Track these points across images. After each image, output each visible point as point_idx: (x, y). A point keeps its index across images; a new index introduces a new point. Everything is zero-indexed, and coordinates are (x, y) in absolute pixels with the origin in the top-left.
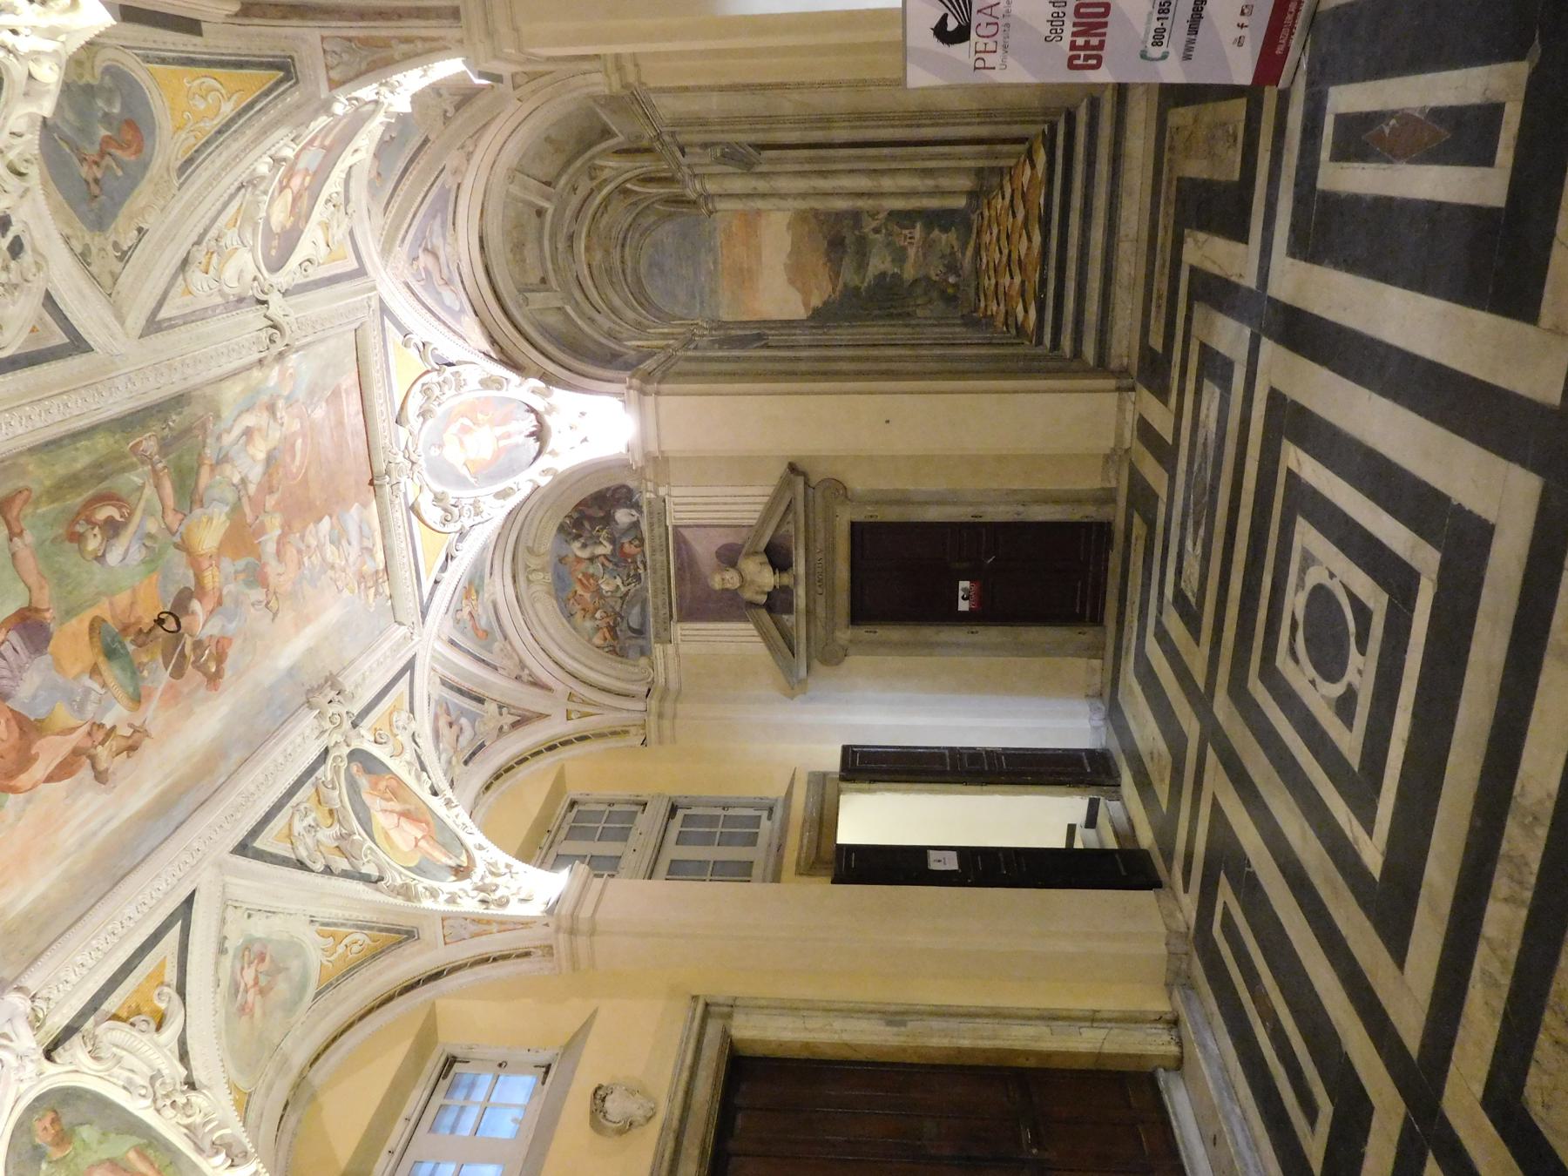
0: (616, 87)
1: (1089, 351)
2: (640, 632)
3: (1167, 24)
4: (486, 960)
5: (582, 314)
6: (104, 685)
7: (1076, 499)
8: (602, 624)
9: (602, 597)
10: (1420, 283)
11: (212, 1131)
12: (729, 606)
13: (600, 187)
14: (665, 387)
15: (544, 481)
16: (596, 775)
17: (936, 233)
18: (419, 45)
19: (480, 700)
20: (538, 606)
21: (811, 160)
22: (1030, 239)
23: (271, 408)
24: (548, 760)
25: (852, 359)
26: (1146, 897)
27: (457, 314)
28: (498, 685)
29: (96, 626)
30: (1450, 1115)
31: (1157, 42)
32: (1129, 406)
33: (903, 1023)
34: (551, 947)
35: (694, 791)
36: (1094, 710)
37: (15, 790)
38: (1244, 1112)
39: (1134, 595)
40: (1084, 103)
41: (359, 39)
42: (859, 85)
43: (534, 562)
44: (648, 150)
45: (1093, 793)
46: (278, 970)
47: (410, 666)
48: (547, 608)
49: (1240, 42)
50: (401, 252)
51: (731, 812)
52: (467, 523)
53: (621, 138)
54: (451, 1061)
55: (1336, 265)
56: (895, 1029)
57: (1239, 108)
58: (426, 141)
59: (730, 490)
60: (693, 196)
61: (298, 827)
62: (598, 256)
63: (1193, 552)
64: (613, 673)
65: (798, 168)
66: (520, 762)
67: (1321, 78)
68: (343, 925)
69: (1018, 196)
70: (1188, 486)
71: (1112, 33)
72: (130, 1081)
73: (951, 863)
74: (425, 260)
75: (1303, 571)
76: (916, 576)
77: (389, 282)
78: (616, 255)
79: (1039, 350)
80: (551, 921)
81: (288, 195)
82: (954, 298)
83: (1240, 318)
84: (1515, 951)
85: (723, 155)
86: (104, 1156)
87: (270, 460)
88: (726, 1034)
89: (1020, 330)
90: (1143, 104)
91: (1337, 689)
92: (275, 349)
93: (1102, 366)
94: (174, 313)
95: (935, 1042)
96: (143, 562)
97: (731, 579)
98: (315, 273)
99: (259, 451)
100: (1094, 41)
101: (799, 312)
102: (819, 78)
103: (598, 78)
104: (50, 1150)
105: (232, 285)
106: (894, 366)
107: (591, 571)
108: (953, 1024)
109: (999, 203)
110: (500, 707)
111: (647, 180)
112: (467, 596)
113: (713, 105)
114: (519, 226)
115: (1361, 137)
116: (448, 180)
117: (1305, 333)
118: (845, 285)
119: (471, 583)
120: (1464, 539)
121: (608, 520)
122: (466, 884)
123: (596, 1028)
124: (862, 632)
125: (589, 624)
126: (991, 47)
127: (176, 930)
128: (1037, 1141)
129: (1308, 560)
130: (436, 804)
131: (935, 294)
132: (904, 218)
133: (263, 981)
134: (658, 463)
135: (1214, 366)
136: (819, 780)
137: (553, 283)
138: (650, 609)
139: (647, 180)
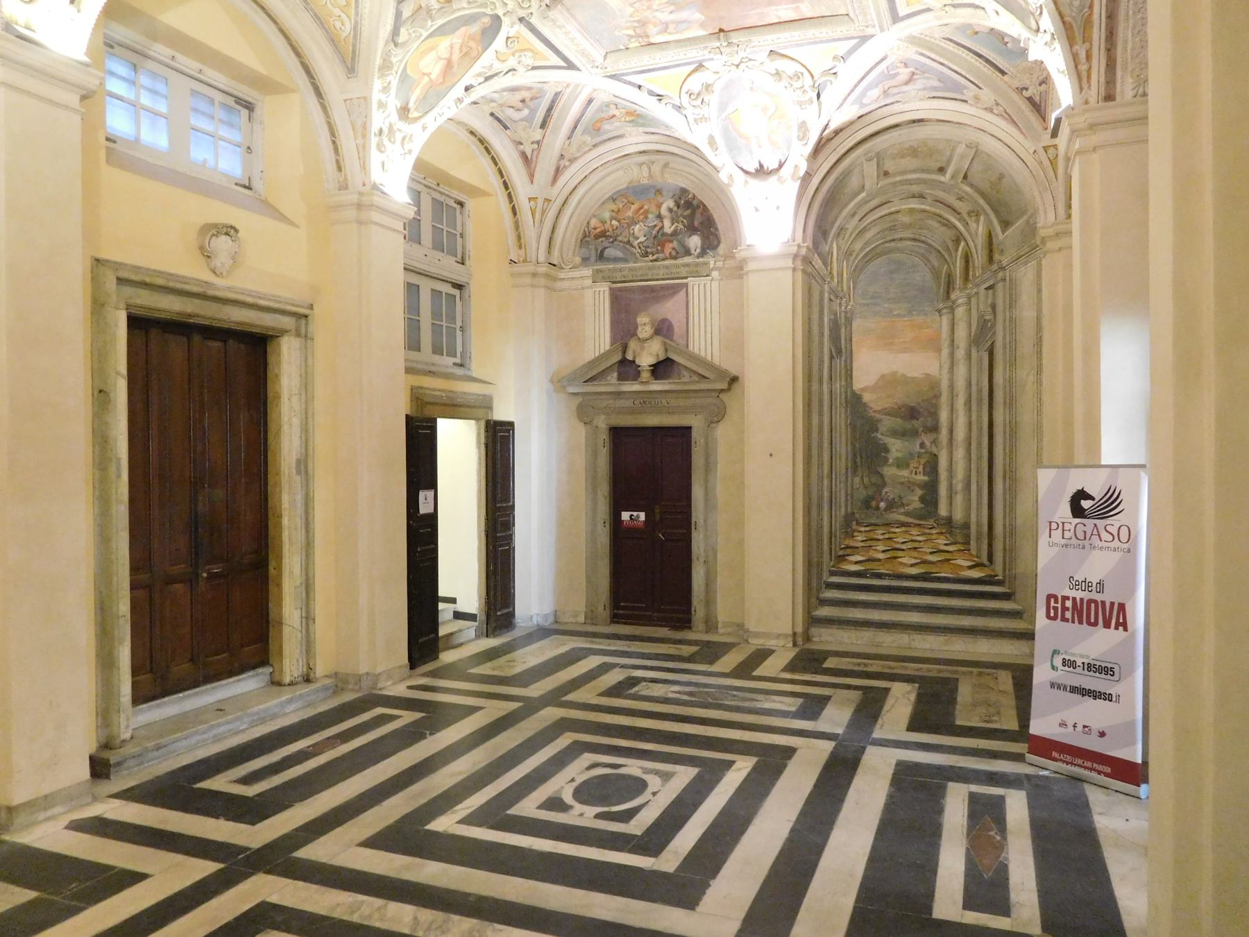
0: (1042, 233)
1: (825, 612)
2: (601, 257)
3: (1079, 670)
4: (333, 134)
5: (859, 206)
7: (709, 602)
8: (607, 226)
9: (629, 225)
10: (875, 859)
12: (623, 330)
13: (961, 220)
14: (799, 275)
15: (723, 177)
16: (485, 222)
17: (919, 492)
18: (1083, 68)
19: (543, 125)
20: (620, 173)
21: (980, 391)
22: (912, 565)
25: (821, 427)
26: (405, 660)
27: (859, 101)
28: (556, 141)
30: (254, 878)
32: (781, 643)
33: (299, 472)
35: (474, 302)
36: (546, 617)
38: (243, 731)
41: (1090, 15)
42: (1038, 430)
43: (656, 169)
44: (991, 259)
45: (482, 617)
47: (570, 66)
50: (911, 53)
51: (459, 333)
52: (689, 111)
53: (1001, 237)
54: (249, 107)
55: (890, 797)
57: (1010, 723)
58: (1003, 73)
59: (716, 331)
60: (953, 297)
62: (906, 219)
63: (670, 691)
64: (568, 234)
65: (974, 382)
66: (493, 159)
67: (1036, 788)
68: (357, 13)
69: (948, 556)
70: (719, 687)
74: (905, 73)
76: (650, 484)
77: (891, 44)
78: (907, 234)
80: (368, 187)
84: (377, 925)
88: (283, 332)
89: (842, 558)
90: (1016, 652)
91: (568, 798)
93: (813, 621)
97: (645, 331)
100: (1068, 615)
101: (858, 385)
103: (1051, 217)
107: (650, 216)
108: (300, 510)
109: (941, 542)
110: (538, 142)
111: (967, 259)
112: (629, 113)
113: (1026, 314)
114: (931, 153)
115: (986, 814)
117: (839, 772)
118: (879, 421)
121: (692, 230)
122: (394, 117)
124: (604, 436)
125: (607, 215)
126: (1067, 535)
128: (212, 576)
130: (458, 90)
131: (871, 492)
132: (932, 467)
134: (739, 270)
135: (813, 706)
136: (486, 404)
137: (885, 182)
139: (967, 259)
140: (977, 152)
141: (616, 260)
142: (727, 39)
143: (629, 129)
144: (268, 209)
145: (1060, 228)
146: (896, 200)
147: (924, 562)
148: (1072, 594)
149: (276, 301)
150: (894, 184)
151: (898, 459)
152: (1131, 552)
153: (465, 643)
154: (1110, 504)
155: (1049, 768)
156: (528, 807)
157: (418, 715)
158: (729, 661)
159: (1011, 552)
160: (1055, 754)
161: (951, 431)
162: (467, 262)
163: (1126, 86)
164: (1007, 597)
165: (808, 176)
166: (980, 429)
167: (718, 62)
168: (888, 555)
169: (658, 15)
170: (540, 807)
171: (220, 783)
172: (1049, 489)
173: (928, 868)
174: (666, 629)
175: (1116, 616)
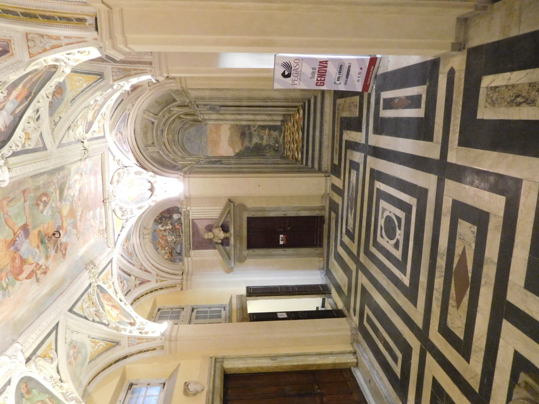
0: (179, 88)
1: (316, 166)
2: (180, 254)
3: (341, 76)
4: (141, 352)
5: (165, 154)
6: (40, 252)
7: (314, 209)
8: (168, 251)
9: (168, 243)
10: (407, 136)
11: (69, 395)
12: (209, 244)
13: (172, 116)
14: (191, 175)
15: (153, 204)
16: (165, 300)
17: (272, 132)
18: (139, 71)
19: (130, 275)
20: (147, 246)
21: (235, 110)
22: (299, 134)
23: (81, 174)
24: (150, 296)
26: (344, 319)
28: (135, 271)
29: (40, 232)
30: (431, 339)
31: (338, 80)
32: (329, 181)
33: (276, 360)
34: (163, 346)
35: (199, 304)
36: (321, 273)
37: (18, 280)
38: (377, 371)
39: (333, 235)
40: (313, 98)
41: (122, 69)
43: (146, 232)
45: (323, 296)
46: (79, 352)
47: (111, 261)
48: (149, 246)
49: (358, 81)
50: (114, 132)
51: (212, 309)
52: (128, 216)
53: (179, 102)
54: (131, 385)
55: (386, 135)
56: (274, 361)
57: (357, 99)
58: (123, 100)
59: (209, 208)
60: (200, 119)
61: (85, 306)
62: (171, 136)
63: (351, 217)
64: (170, 267)
65: (232, 112)
66: (141, 296)
67: (380, 89)
68: (98, 339)
69: (295, 122)
70: (348, 200)
71: (327, 78)
72: (45, 377)
73: (285, 316)
74: (119, 135)
75: (383, 213)
76: (268, 233)
77: (111, 139)
78: (176, 136)
79: (302, 166)
80: (162, 337)
81: (93, 111)
82: (278, 150)
83: (361, 151)
84: (442, 289)
85: (210, 108)
86: (40, 399)
87: (80, 191)
88: (222, 367)
89: (297, 160)
90: (329, 98)
91: (394, 241)
92: (86, 156)
93: (320, 170)
94: (65, 142)
95: (286, 364)
96: (51, 215)
98: (96, 135)
99: (78, 186)
100: (323, 79)
101: (232, 154)
102: (238, 87)
104: (25, 395)
105: (78, 136)
106: (260, 170)
107: (165, 234)
108: (290, 359)
109: (290, 124)
110: (136, 278)
111: (186, 114)
113: (207, 94)
114: (146, 127)
115: (389, 104)
116: (127, 112)
117: (379, 153)
118: (246, 146)
119: (127, 237)
120: (421, 194)
121: (171, 217)
122: (134, 327)
123: (180, 369)
124: (251, 251)
125: (163, 252)
126: (296, 79)
127: (55, 332)
128: (319, 388)
129: (384, 210)
130: (122, 304)
131: (272, 149)
132: (263, 127)
133: (75, 354)
134: (188, 199)
135: (354, 165)
136: (240, 297)
138: (184, 246)
139: (186, 114)
140: (147, 110)
141: (181, 248)
142: (106, 199)
143: (131, 242)
144: (173, 376)
145: (178, 81)
146: (163, 140)
147: (297, 130)
148: (316, 78)
149: (211, 368)
150: (157, 140)
151: (260, 140)
152: (303, 59)
153: (336, 301)
154: (287, 66)
155: (373, 87)
156: (398, 254)
157: (366, 307)
158: (337, 199)
159: (294, 100)
160: (368, 83)
161: (250, 121)
162: (182, 307)
163: (148, 58)
164: (309, 101)
165: (153, 172)
166: (248, 110)
167: (114, 204)
168: (295, 142)
169: (97, 224)
170: (398, 250)
171: (397, 370)
172: (281, 84)
173: (408, 120)
174: (325, 226)
175: (323, 64)
